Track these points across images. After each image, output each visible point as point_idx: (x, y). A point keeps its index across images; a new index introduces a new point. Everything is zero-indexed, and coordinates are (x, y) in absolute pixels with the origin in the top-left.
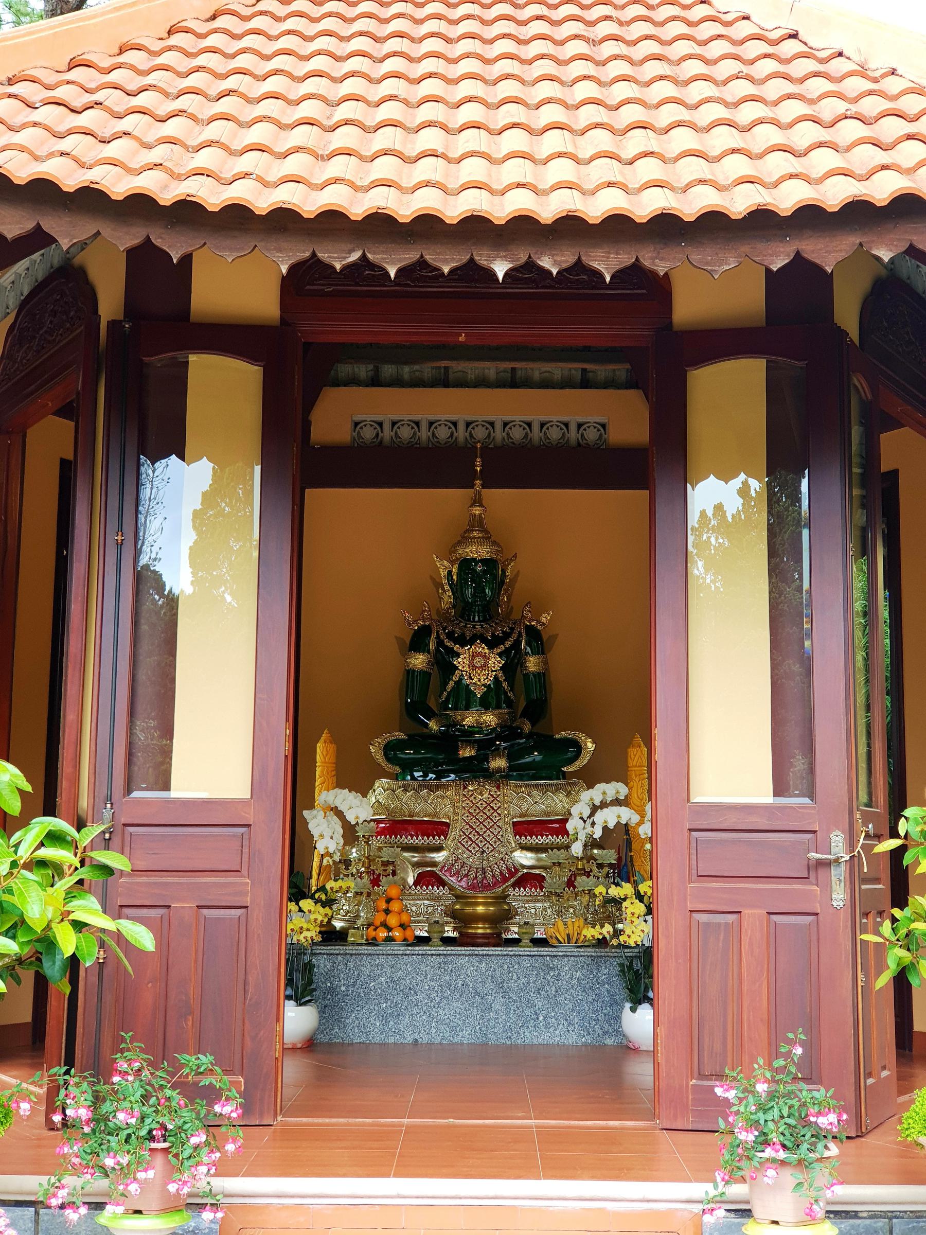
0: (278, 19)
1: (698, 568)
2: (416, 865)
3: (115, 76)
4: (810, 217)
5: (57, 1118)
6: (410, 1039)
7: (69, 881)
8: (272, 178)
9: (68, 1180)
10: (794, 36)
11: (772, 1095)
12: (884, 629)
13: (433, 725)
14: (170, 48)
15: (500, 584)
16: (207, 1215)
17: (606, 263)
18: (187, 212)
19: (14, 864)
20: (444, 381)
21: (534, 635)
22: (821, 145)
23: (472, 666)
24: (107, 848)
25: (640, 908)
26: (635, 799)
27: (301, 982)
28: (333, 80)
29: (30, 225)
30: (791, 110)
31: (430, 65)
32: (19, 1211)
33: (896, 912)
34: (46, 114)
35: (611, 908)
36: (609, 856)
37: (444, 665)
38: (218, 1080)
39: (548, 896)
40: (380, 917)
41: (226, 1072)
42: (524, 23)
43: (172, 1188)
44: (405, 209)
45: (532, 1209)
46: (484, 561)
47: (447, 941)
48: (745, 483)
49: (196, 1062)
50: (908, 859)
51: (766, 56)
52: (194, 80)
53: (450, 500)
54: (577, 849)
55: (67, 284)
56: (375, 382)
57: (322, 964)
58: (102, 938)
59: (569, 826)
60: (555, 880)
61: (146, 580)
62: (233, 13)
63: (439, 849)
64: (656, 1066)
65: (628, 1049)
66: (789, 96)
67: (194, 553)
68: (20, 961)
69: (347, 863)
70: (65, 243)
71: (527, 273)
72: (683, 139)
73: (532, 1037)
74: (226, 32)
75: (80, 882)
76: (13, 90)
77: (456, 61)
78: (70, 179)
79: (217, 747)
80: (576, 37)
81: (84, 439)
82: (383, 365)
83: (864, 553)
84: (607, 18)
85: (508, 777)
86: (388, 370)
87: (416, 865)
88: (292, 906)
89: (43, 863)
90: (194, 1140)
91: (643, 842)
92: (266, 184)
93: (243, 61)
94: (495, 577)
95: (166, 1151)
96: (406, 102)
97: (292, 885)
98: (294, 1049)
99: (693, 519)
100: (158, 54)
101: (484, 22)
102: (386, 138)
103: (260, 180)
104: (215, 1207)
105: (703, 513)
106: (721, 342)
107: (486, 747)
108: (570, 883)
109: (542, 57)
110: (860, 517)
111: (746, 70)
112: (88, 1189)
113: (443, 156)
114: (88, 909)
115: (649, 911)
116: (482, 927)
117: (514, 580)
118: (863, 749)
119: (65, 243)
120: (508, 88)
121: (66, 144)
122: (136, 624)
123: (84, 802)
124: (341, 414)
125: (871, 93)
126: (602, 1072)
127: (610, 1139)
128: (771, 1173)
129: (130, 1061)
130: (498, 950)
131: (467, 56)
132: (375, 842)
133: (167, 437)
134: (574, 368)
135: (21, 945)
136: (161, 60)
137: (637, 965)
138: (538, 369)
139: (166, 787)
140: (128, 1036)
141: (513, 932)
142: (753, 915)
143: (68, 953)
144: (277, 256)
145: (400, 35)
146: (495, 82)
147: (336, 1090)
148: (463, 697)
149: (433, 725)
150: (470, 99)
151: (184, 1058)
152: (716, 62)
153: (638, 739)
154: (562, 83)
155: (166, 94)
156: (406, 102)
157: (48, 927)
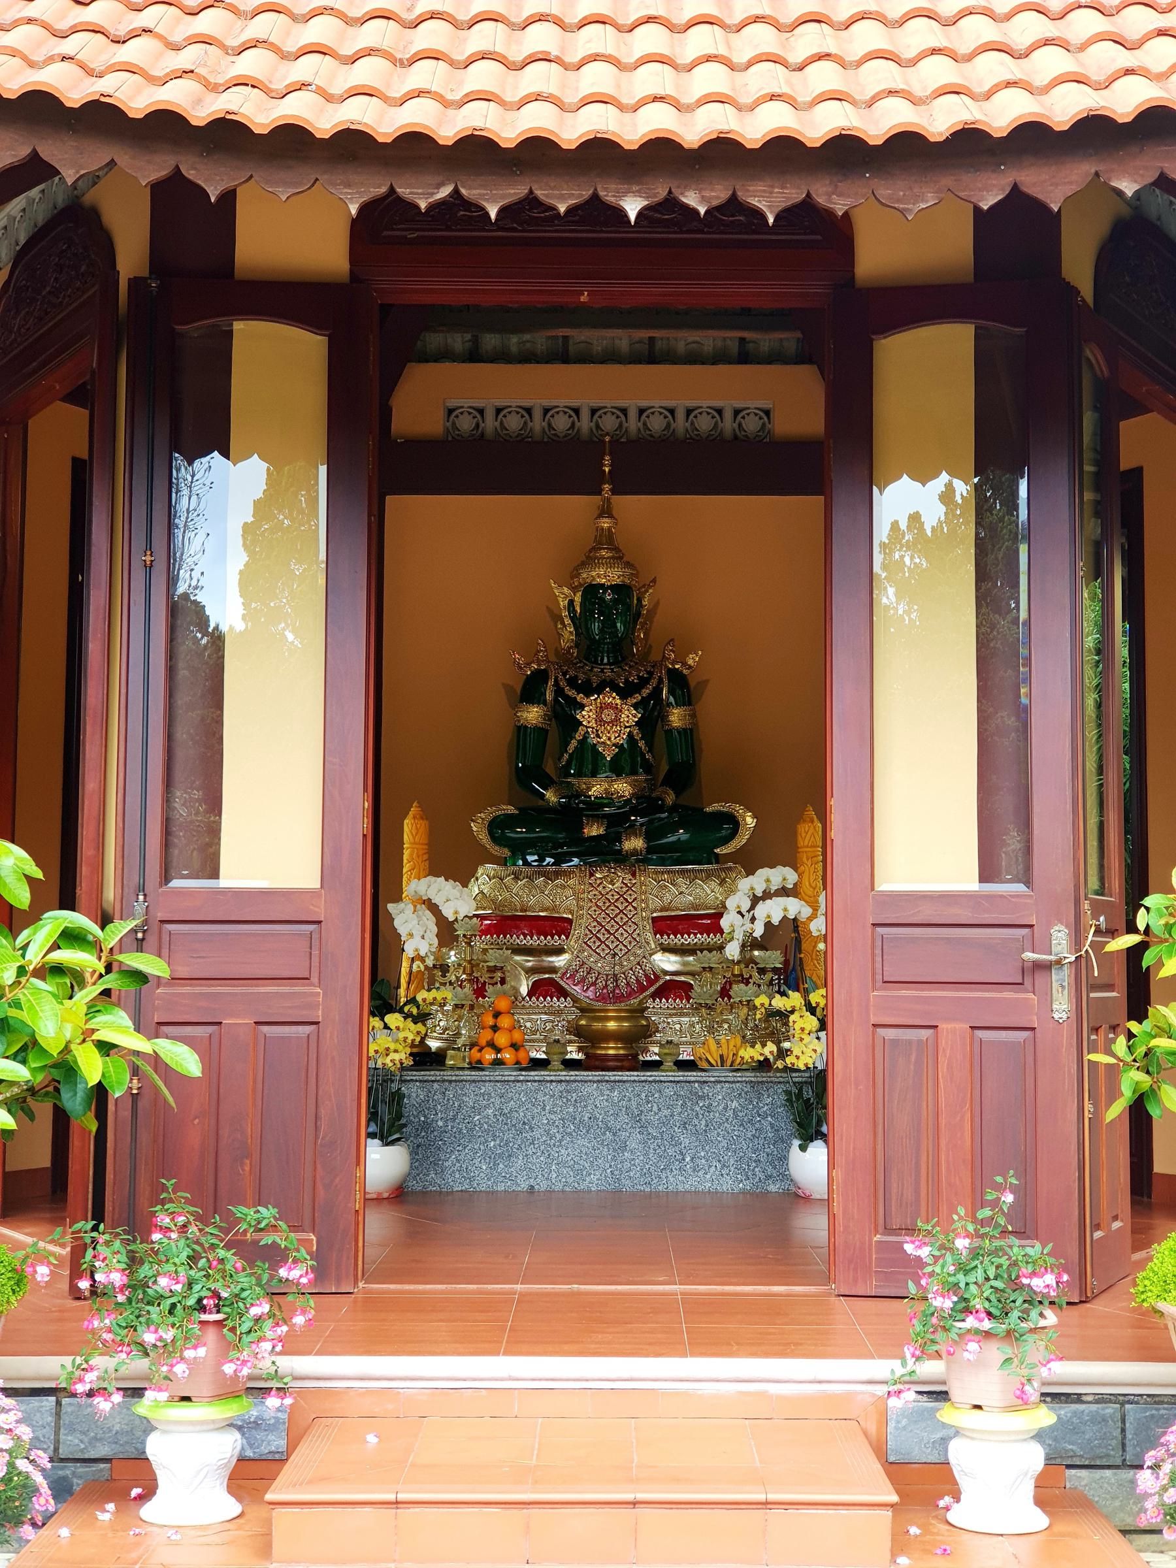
1: (887, 597)
2: (530, 971)
4: (1032, 138)
5: (84, 1284)
6: (524, 1186)
7: (91, 991)
11: (975, 1253)
13: (551, 796)
15: (634, 616)
16: (273, 1402)
17: (768, 200)
18: (227, 134)
19: (21, 971)
20: (562, 355)
21: (678, 681)
22: (1047, 42)
23: (600, 721)
24: (140, 949)
25: (812, 1022)
26: (806, 888)
27: (387, 1115)
29: (24, 152)
32: (35, 1402)
33: (1133, 1026)
35: (775, 1023)
36: (773, 958)
37: (564, 719)
39: (697, 1008)
40: (486, 1035)
41: (293, 1228)
43: (229, 1369)
44: (508, 130)
45: (677, 1394)
46: (615, 588)
47: (570, 1064)
48: (949, 487)
50: (1148, 959)
53: (572, 509)
54: (733, 951)
55: (75, 229)
56: (474, 356)
57: (414, 1093)
58: (135, 1063)
59: (724, 923)
60: (704, 989)
61: (184, 614)
63: (559, 951)
64: (832, 1218)
65: (797, 1197)
67: (246, 580)
68: (32, 1091)
69: (444, 969)
70: (70, 175)
71: (667, 211)
73: (676, 1182)
75: (106, 993)
78: (75, 91)
79: (278, 823)
81: (101, 432)
82: (484, 334)
85: (646, 861)
86: (490, 341)
87: (530, 971)
88: (376, 1022)
89: (58, 970)
90: (255, 1311)
92: (329, 98)
94: (629, 607)
95: (220, 1324)
97: (375, 995)
98: (379, 1200)
99: (881, 532)
103: (321, 92)
105: (895, 525)
106: (917, 302)
107: (618, 823)
108: (725, 993)
110: (1093, 528)
112: (124, 1370)
113: (558, 61)
114: (117, 1027)
115: (823, 1026)
116: (612, 1044)
117: (652, 612)
118: (1093, 821)
119: (70, 175)
122: (167, 844)
123: (110, 894)
126: (764, 1226)
127: (773, 1309)
128: (973, 1346)
130: (634, 1075)
132: (479, 943)
133: (208, 430)
134: (729, 338)
135: (34, 1071)
137: (808, 1093)
138: (684, 339)
139: (215, 874)
140: (170, 1184)
141: (653, 1053)
142: (953, 1030)
143: (93, 1081)
144: (344, 193)
147: (430, 1248)
148: (589, 760)
149: (551, 796)
151: (240, 1211)
157: (67, 1050)
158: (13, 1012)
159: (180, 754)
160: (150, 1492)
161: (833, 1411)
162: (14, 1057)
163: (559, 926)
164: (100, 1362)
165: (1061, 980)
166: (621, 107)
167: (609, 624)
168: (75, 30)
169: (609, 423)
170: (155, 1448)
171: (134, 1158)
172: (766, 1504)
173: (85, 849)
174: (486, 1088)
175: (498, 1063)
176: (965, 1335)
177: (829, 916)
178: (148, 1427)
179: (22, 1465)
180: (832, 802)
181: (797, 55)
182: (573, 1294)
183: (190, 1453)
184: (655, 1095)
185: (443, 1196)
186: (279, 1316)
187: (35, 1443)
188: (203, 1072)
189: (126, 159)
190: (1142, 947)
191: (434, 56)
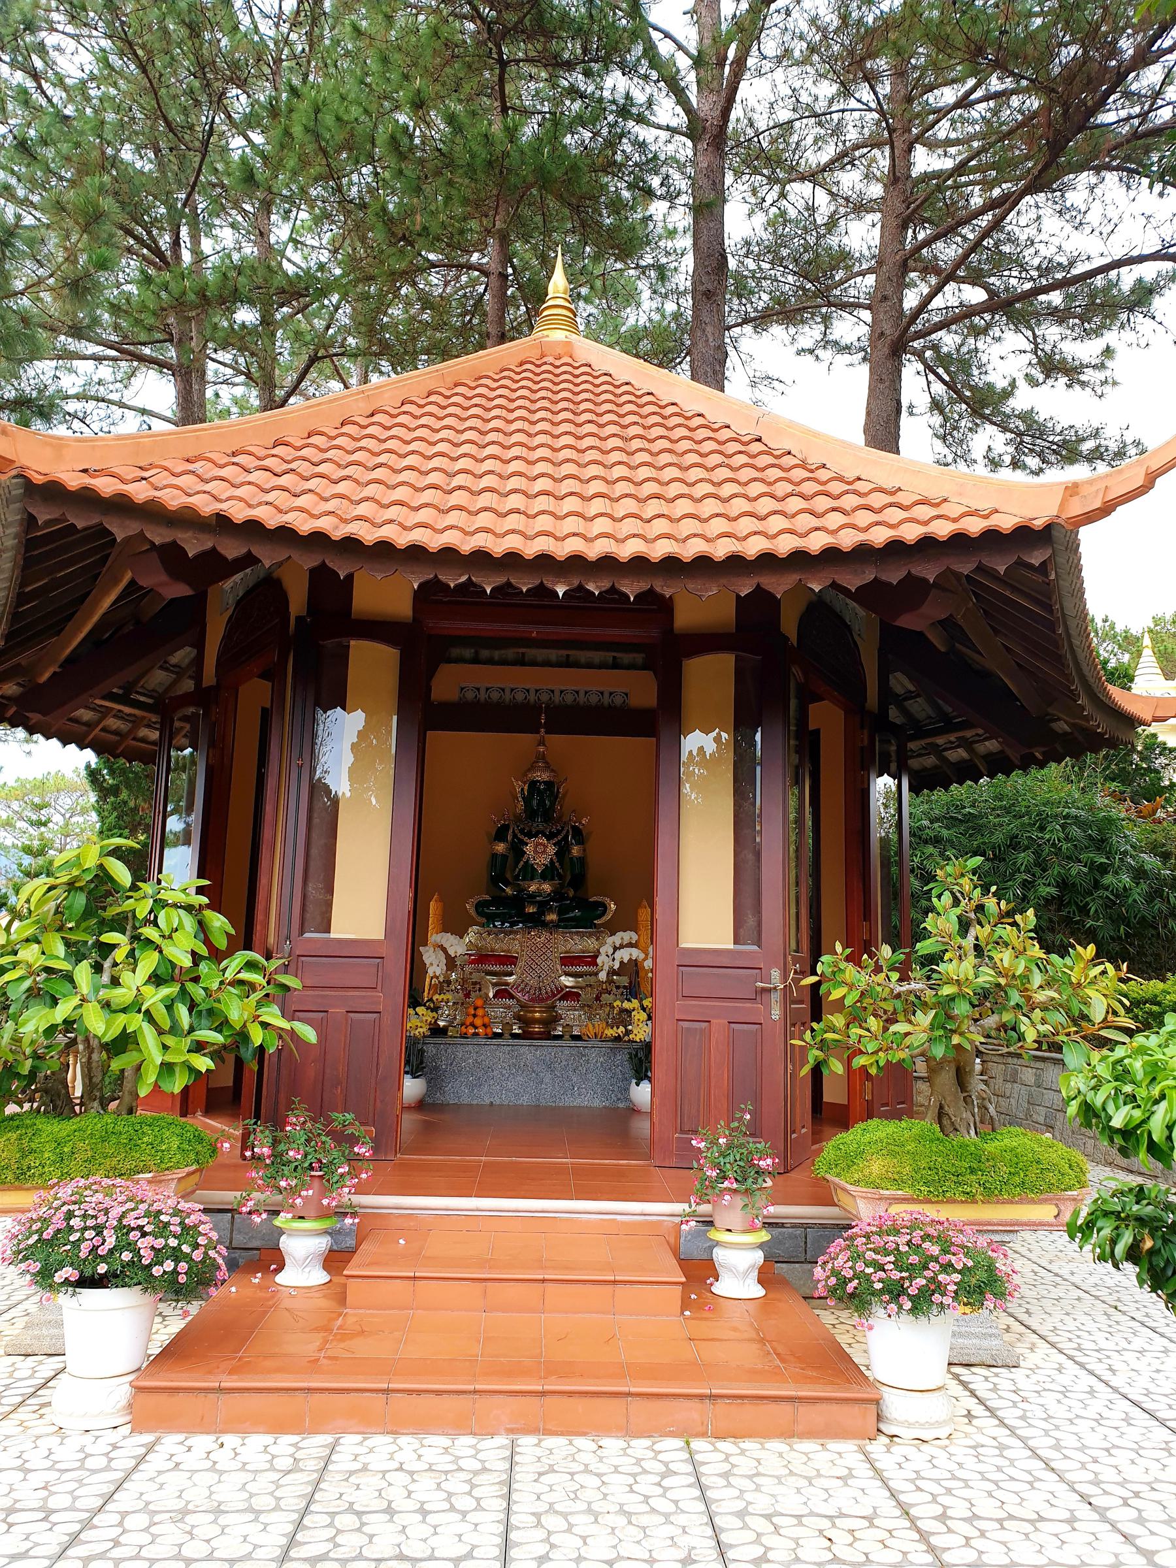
0: (416, 417)
1: (687, 788)
2: (494, 985)
4: (767, 560)
5: (248, 1154)
7: (259, 995)
9: (255, 1195)
10: (759, 440)
11: (729, 1146)
12: (809, 834)
13: (509, 891)
14: (342, 435)
15: (555, 797)
16: (348, 1221)
17: (631, 589)
18: (351, 544)
19: (222, 983)
20: (521, 662)
21: (577, 832)
22: (775, 512)
23: (535, 852)
25: (643, 1016)
26: (642, 943)
27: (416, 1062)
28: (452, 459)
29: (244, 551)
30: (756, 489)
31: (516, 451)
33: (815, 1025)
35: (624, 1016)
36: (624, 981)
37: (517, 850)
38: (356, 1130)
39: (582, 1007)
40: (470, 1020)
41: (362, 1124)
42: (580, 425)
43: (325, 1202)
44: (498, 548)
45: (567, 1219)
47: (515, 1036)
48: (719, 734)
49: (343, 1118)
52: (357, 456)
53: (525, 740)
54: (603, 976)
55: (269, 589)
56: (476, 660)
57: (430, 1050)
59: (599, 961)
60: (587, 996)
61: (318, 789)
63: (511, 974)
64: (652, 1124)
65: (633, 1111)
66: (755, 480)
67: (352, 770)
68: (224, 1047)
69: (449, 983)
70: (267, 563)
71: (578, 594)
72: (683, 506)
73: (568, 1101)
74: (380, 424)
75: (267, 995)
76: (235, 460)
77: (534, 449)
78: (272, 520)
79: (363, 900)
80: (614, 435)
81: (278, 695)
82: (482, 650)
83: (797, 783)
85: (557, 926)
86: (485, 653)
87: (494, 985)
88: (411, 1011)
89: (242, 982)
91: (647, 972)
92: (405, 528)
93: (391, 444)
94: (552, 792)
96: (500, 475)
97: (411, 996)
99: (684, 758)
100: (334, 438)
102: (486, 500)
103: (400, 524)
104: (354, 1215)
106: (706, 642)
107: (543, 907)
108: (598, 998)
109: (592, 448)
110: (795, 759)
113: (525, 513)
114: (273, 1015)
115: (650, 1018)
116: (537, 1025)
117: (565, 795)
118: (793, 911)
119: (267, 563)
120: (569, 469)
121: (270, 497)
123: (271, 940)
124: (448, 683)
125: (809, 479)
126: (616, 1126)
127: (619, 1173)
128: (727, 1197)
129: (297, 1117)
131: (542, 445)
132: (468, 969)
133: (336, 697)
134: (608, 656)
135: (226, 1037)
136: (398, 420)
137: (641, 1054)
138: (583, 656)
143: (257, 1044)
144: (411, 577)
145: (497, 430)
146: (560, 464)
147: (438, 1137)
148: (529, 872)
149: (509, 891)
151: (334, 1115)
152: (707, 455)
154: (605, 466)
155: (339, 465)
156: (500, 475)
157: (244, 1026)
158: (216, 1005)
159: (312, 864)
160: (281, 1267)
162: (215, 1030)
164: (255, 1195)
167: (541, 803)
168: (273, 489)
169: (545, 698)
170: (285, 1243)
172: (615, 1282)
173: (259, 916)
175: (476, 1034)
178: (281, 1232)
179: (212, 1253)
180: (657, 899)
183: (303, 1251)
184: (561, 1052)
187: (219, 1242)
188: (343, 657)
189: (296, 556)
190: (819, 984)
191: (460, 508)
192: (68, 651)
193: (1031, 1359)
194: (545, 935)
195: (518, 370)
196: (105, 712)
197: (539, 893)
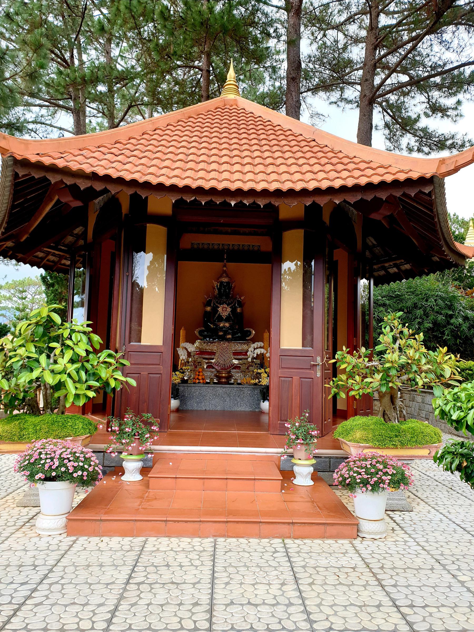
0: (173, 131)
1: (283, 284)
2: (207, 363)
3: (128, 146)
4: (317, 191)
5: (110, 430)
6: (204, 409)
7: (113, 367)
8: (170, 176)
10: (314, 140)
11: (300, 426)
13: (212, 326)
14: (143, 139)
15: (230, 288)
16: (150, 456)
18: (147, 185)
19: (98, 362)
22: (321, 171)
24: (124, 358)
25: (266, 375)
26: (265, 346)
27: (176, 393)
30: (313, 161)
32: (99, 454)
33: (334, 379)
34: (108, 156)
35: (258, 375)
36: (258, 361)
37: (215, 310)
38: (152, 420)
39: (242, 372)
40: (197, 377)
41: (155, 418)
43: (140, 448)
48: (297, 263)
50: (338, 365)
51: (306, 146)
53: (218, 265)
55: (114, 202)
57: (181, 389)
58: (122, 382)
59: (248, 354)
61: (134, 285)
62: (160, 129)
63: (213, 359)
64: (269, 417)
65: (262, 412)
68: (100, 387)
69: (188, 362)
74: (158, 134)
76: (99, 149)
78: (115, 175)
79: (154, 329)
80: (255, 138)
84: (263, 133)
87: (207, 363)
88: (173, 373)
89: (106, 362)
90: (146, 436)
91: (267, 358)
92: (169, 178)
93: (163, 143)
95: (139, 439)
96: (208, 155)
98: (173, 411)
101: (230, 134)
102: (202, 166)
103: (167, 176)
104: (152, 453)
105: (285, 270)
106: (292, 224)
107: (226, 333)
108: (248, 368)
111: (301, 149)
112: (118, 448)
113: (218, 171)
115: (268, 376)
116: (224, 378)
119: (113, 193)
121: (114, 165)
122: (130, 333)
123: (117, 345)
124: (189, 240)
125: (334, 157)
126: (254, 419)
127: (257, 437)
128: (299, 446)
129: (129, 415)
130: (228, 386)
131: (225, 143)
133: (141, 247)
136: (140, 142)
138: (242, 230)
139: (140, 341)
140: (129, 408)
141: (232, 381)
142: (296, 378)
144: (172, 198)
147: (184, 422)
148: (220, 319)
150: (225, 155)
151: (144, 414)
152: (293, 147)
153: (266, 331)
155: (142, 152)
156: (208, 155)
157: (107, 379)
158: (96, 371)
159: (133, 315)
160: (123, 474)
161: (269, 458)
162: (96, 381)
163: (214, 354)
164: (113, 446)
165: (319, 368)
166: (231, 182)
168: (115, 162)
170: (125, 464)
171: (121, 402)
172: (255, 479)
174: (197, 388)
175: (199, 382)
176: (297, 444)
177: (270, 353)
178: (123, 460)
179: (96, 468)
180: (272, 330)
181: (268, 172)
182: (214, 433)
183: (132, 466)
184: (233, 390)
185: (187, 411)
186: (151, 437)
187: (99, 464)
191: (191, 169)
192: (32, 229)
193: (417, 509)
194: (227, 344)
195: (215, 111)
196: (48, 253)
197: (224, 327)
